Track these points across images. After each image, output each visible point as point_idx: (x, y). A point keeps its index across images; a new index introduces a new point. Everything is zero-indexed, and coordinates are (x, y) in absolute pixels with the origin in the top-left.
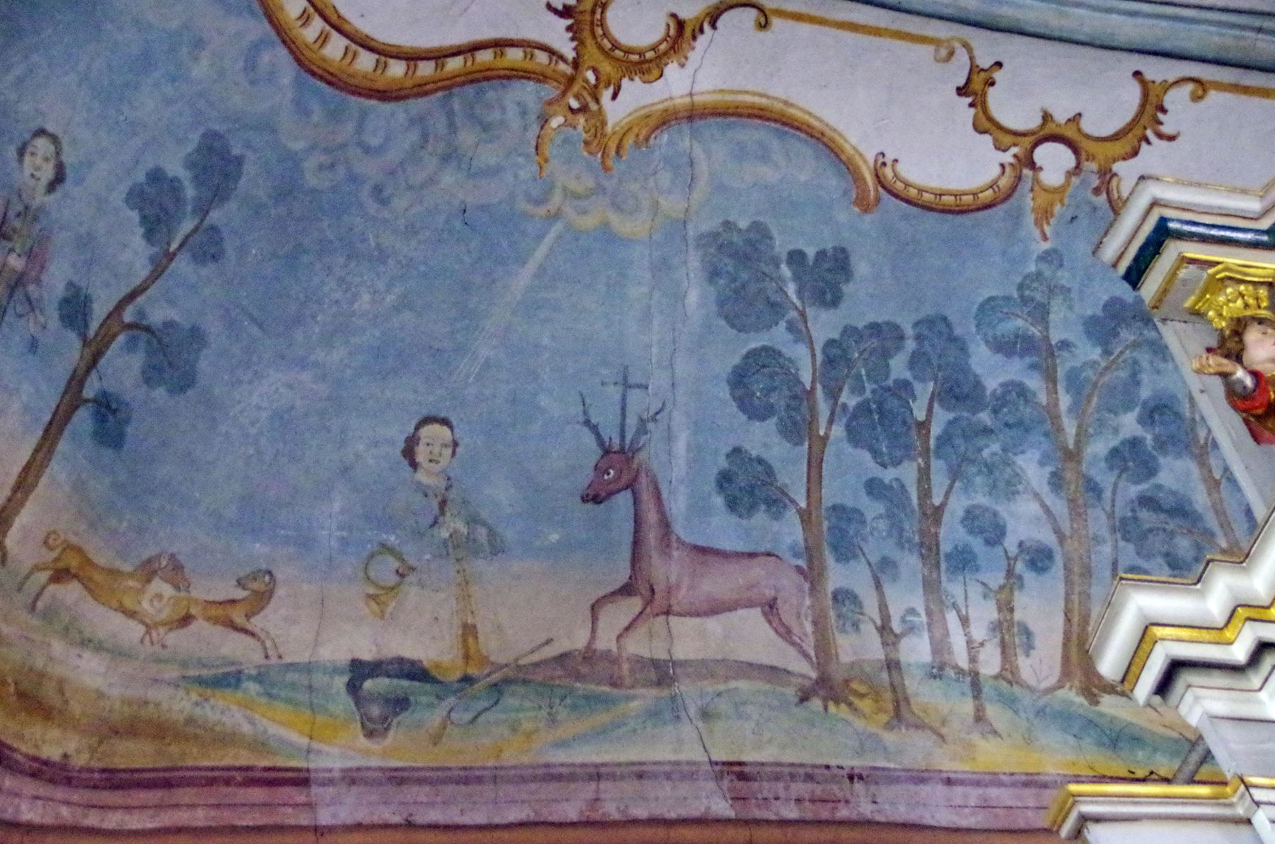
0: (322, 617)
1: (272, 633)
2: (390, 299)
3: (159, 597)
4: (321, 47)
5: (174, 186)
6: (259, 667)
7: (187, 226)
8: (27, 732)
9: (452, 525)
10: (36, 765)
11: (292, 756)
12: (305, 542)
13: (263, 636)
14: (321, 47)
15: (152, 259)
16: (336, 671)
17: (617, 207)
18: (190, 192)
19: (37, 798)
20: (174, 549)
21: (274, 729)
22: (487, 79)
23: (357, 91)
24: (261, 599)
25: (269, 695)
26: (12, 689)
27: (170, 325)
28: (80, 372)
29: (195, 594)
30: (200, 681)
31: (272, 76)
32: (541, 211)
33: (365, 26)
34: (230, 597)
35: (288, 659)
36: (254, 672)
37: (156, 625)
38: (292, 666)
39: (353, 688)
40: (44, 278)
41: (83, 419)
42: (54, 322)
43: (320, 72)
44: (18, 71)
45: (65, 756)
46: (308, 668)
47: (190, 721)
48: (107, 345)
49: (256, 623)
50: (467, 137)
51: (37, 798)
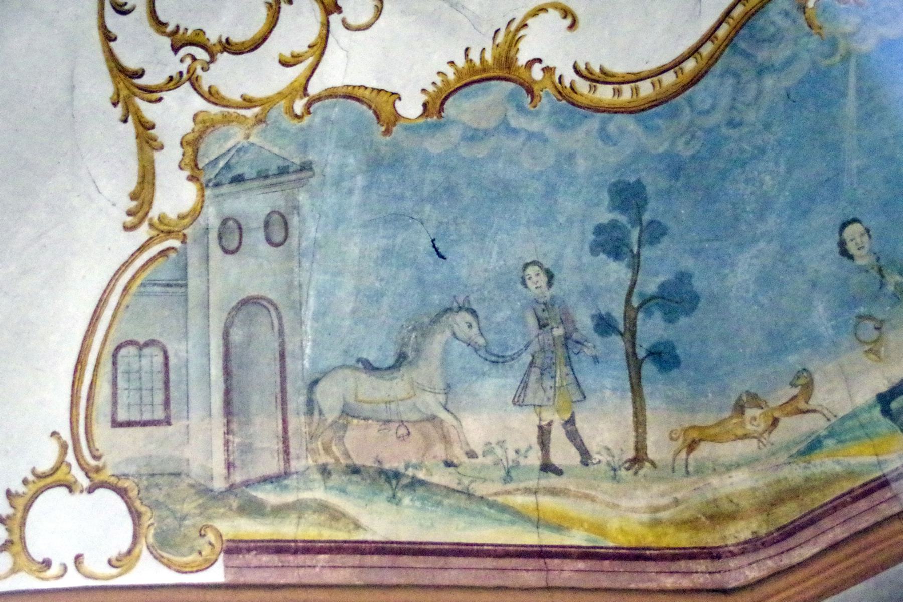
0: (847, 380)
1: (824, 404)
2: (782, 169)
3: (754, 419)
4: (637, 95)
5: (614, 225)
6: (827, 428)
7: (635, 234)
8: (727, 533)
9: (892, 280)
10: (740, 547)
11: (870, 472)
12: (814, 340)
13: (818, 409)
14: (637, 95)
15: (628, 266)
16: (871, 407)
17: (883, 23)
18: (623, 219)
19: (750, 564)
20: (747, 388)
21: (853, 461)
22: (750, 18)
23: (677, 94)
24: (808, 388)
25: (841, 442)
26: (704, 519)
27: (663, 286)
28: (630, 350)
29: (773, 403)
30: (802, 453)
31: (622, 131)
32: (838, 58)
33: (654, 65)
34: (790, 396)
35: (841, 415)
36: (825, 433)
37: (761, 435)
38: (844, 419)
39: (887, 412)
40: (578, 325)
41: (649, 369)
42: (597, 339)
43: (647, 106)
44: (496, 249)
45: (754, 533)
46: (853, 415)
47: (807, 479)
48: (635, 325)
49: (813, 403)
50: (762, 55)
51: (750, 564)
